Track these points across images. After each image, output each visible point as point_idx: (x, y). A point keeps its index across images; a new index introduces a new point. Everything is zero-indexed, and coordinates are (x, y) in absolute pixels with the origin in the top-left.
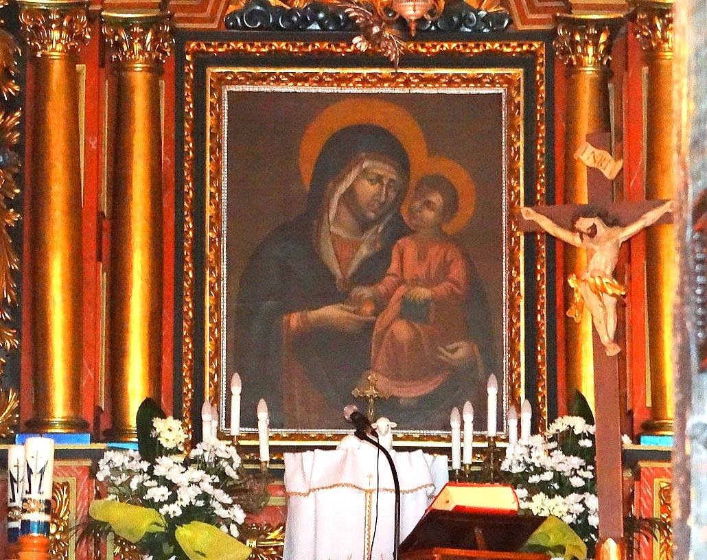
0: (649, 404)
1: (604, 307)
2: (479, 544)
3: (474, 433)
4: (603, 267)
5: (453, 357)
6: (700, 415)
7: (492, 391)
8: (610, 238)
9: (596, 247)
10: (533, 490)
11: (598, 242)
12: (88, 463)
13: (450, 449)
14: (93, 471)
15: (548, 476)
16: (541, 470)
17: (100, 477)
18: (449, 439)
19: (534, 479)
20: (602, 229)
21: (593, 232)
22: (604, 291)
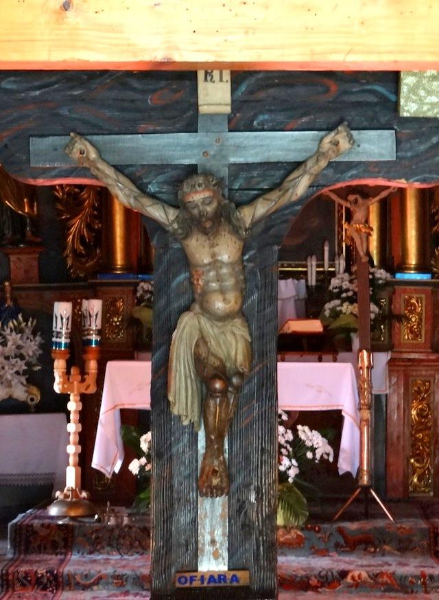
0: (401, 254)
1: (361, 238)
2: (153, 255)
3: (317, 269)
4: (360, 218)
5: (332, 452)
6: (24, 485)
7: (326, 249)
8: (364, 204)
9: (357, 209)
10: (344, 300)
11: (358, 207)
12: (131, 288)
13: (305, 273)
14: (135, 291)
15: (350, 294)
16: (347, 290)
17: (138, 295)
18: (306, 267)
19: (344, 295)
20: (360, 200)
21: (356, 201)
22: (361, 231)
